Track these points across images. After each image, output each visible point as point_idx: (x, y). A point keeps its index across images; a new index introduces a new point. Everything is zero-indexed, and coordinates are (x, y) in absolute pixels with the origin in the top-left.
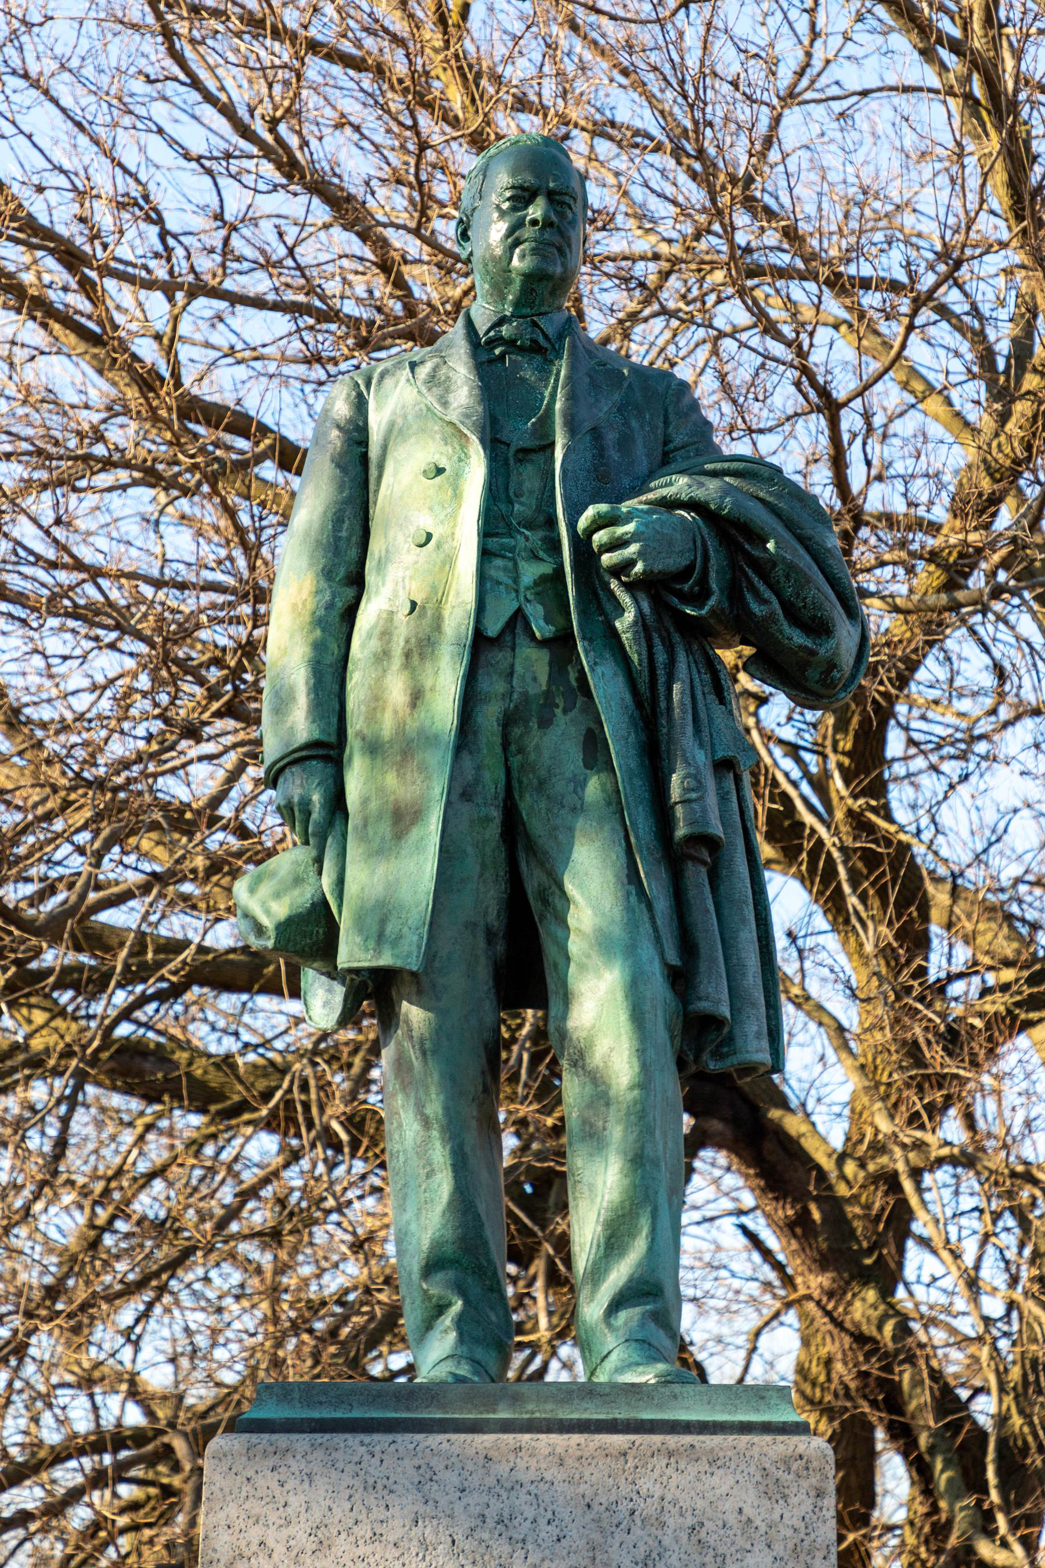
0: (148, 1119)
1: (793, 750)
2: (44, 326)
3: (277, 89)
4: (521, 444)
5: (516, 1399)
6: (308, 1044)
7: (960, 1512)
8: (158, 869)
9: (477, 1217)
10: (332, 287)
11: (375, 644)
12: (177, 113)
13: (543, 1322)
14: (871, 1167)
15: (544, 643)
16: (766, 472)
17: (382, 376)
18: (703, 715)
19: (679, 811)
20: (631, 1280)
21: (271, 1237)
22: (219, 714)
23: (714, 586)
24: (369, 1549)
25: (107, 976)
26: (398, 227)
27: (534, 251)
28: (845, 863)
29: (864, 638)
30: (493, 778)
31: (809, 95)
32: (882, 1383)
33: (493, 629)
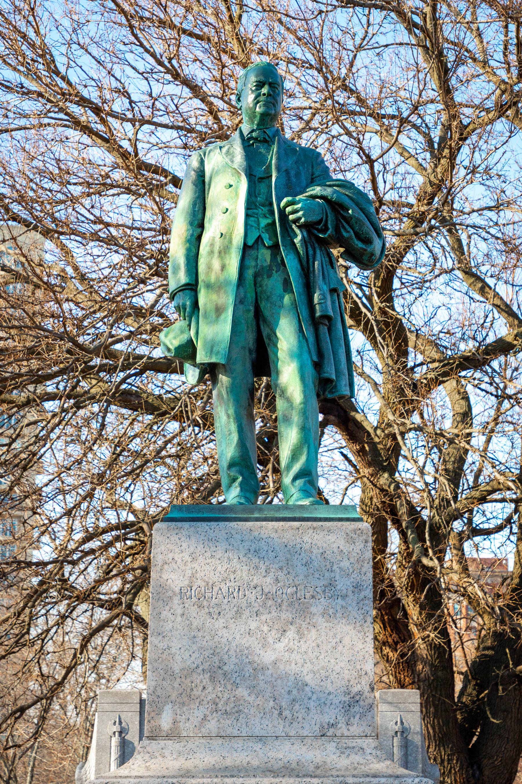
0: (133, 417)
1: (360, 286)
2: (89, 136)
3: (171, 47)
4: (260, 176)
5: (260, 510)
6: (187, 390)
7: (417, 548)
8: (133, 329)
9: (247, 449)
10: (192, 121)
11: (208, 249)
12: (137, 58)
13: (271, 485)
14: (386, 432)
15: (269, 248)
16: (349, 185)
17: (210, 152)
18: (326, 273)
19: (317, 307)
20: (300, 470)
21: (178, 456)
22: (152, 275)
23: (330, 226)
24: (210, 561)
25: (116, 367)
26: (215, 97)
27: (264, 105)
28: (377, 326)
29: (384, 245)
30: (251, 296)
31: (366, 47)
32: (390, 505)
33: (250, 243)
